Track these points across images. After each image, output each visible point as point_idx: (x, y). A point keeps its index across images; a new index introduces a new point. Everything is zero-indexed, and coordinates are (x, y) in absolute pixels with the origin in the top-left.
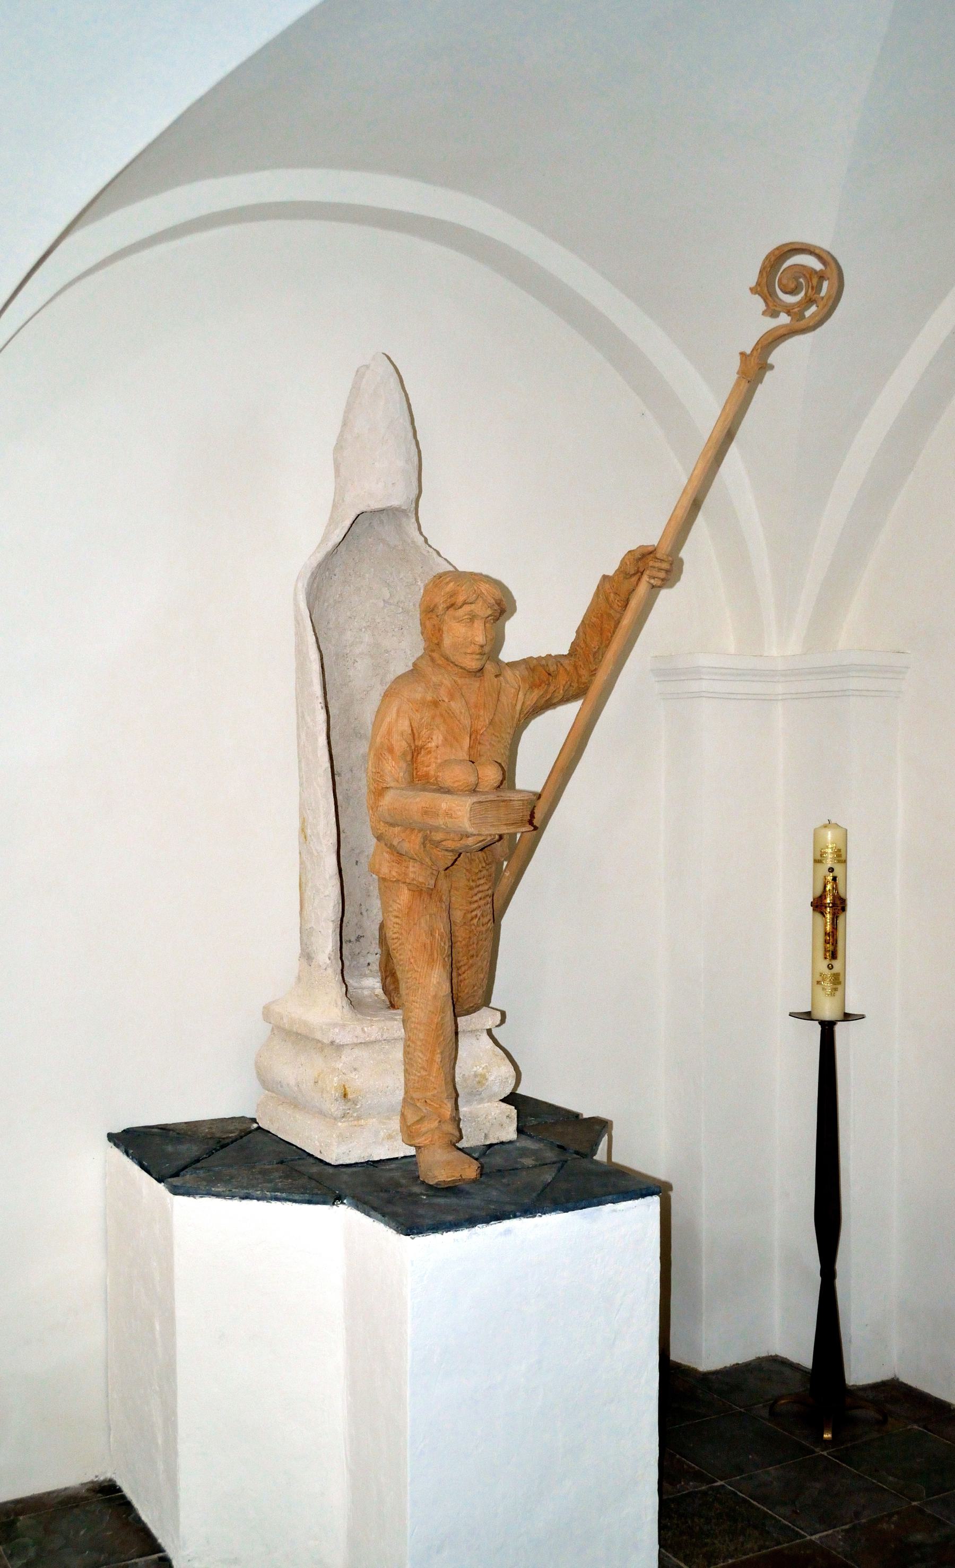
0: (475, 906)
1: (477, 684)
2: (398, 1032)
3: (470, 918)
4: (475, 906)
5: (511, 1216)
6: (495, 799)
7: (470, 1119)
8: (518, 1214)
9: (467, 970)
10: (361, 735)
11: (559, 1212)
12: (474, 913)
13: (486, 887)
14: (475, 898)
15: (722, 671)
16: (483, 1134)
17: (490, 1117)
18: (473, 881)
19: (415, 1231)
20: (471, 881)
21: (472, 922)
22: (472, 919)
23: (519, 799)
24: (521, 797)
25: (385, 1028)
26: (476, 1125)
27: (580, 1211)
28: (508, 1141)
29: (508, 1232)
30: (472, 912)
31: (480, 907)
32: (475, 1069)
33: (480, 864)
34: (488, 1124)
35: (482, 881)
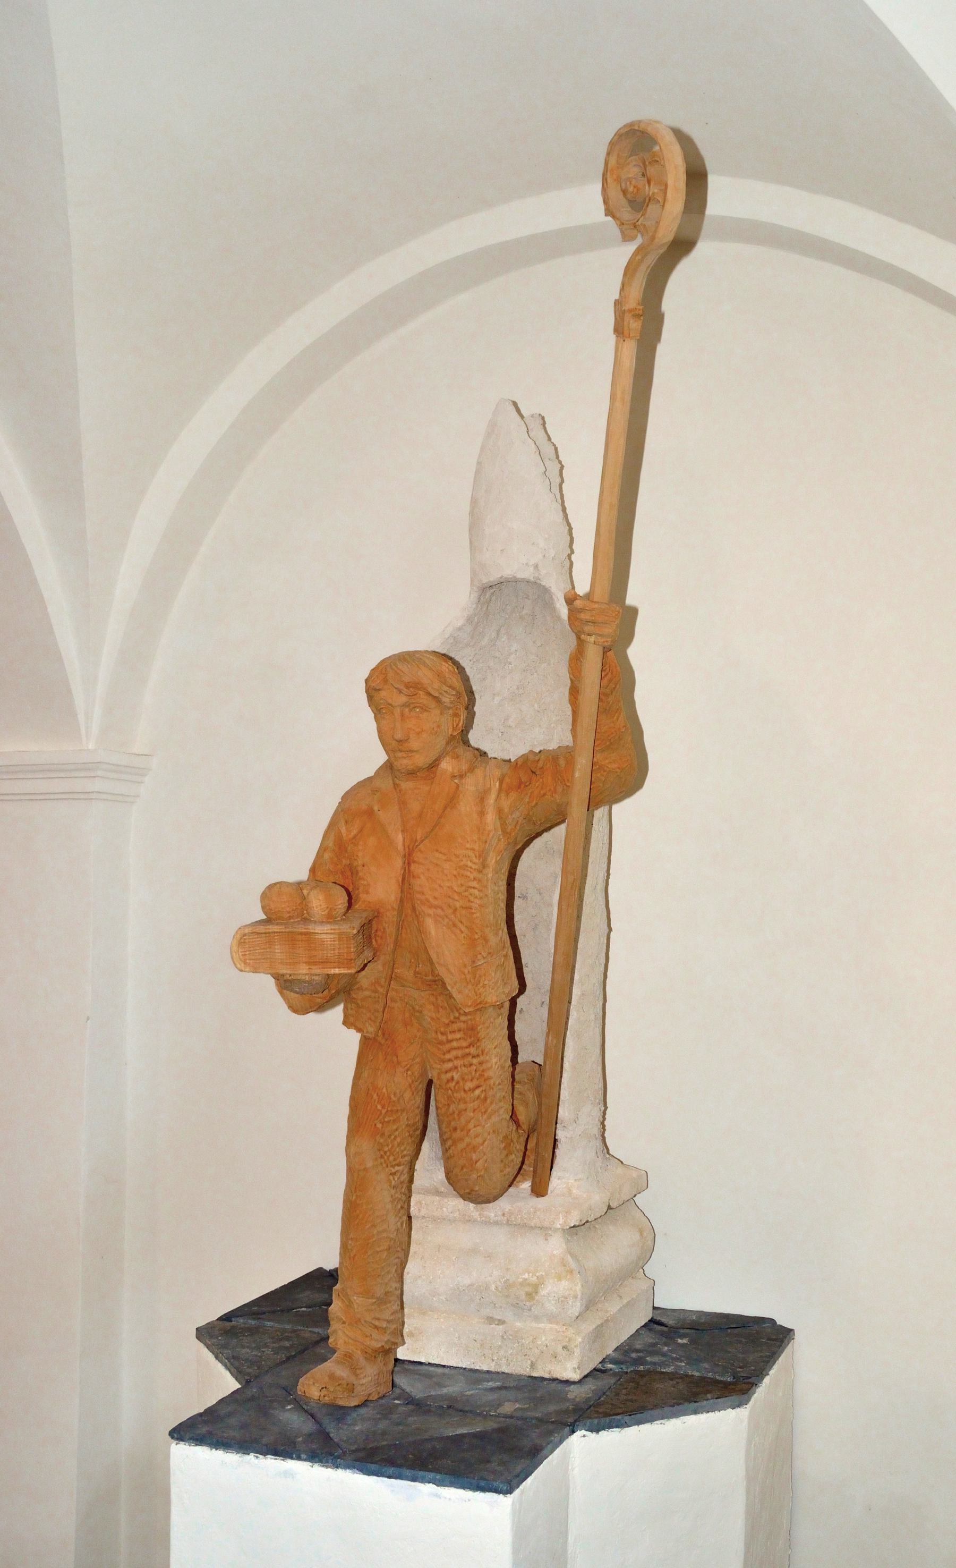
0: (450, 1065)
1: (427, 788)
2: (439, 1210)
3: (446, 1081)
4: (450, 1065)
5: (294, 1456)
6: (284, 930)
7: (511, 1337)
8: (303, 1456)
9: (452, 1146)
10: (554, 851)
11: (357, 1471)
12: (449, 1075)
13: (464, 1044)
14: (448, 1056)
15: (62, 775)
16: (529, 1362)
17: (539, 1343)
18: (442, 1034)
19: (176, 1435)
20: (439, 1034)
21: (448, 1086)
22: (448, 1081)
23: (326, 932)
24: (327, 930)
25: (424, 1202)
26: (520, 1348)
27: (386, 1479)
28: (564, 1379)
29: (287, 1474)
30: (446, 1072)
31: (456, 1068)
32: (526, 1276)
33: (451, 1014)
34: (537, 1351)
35: (458, 1036)
